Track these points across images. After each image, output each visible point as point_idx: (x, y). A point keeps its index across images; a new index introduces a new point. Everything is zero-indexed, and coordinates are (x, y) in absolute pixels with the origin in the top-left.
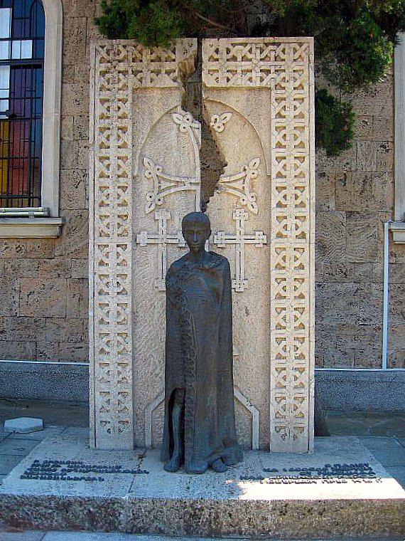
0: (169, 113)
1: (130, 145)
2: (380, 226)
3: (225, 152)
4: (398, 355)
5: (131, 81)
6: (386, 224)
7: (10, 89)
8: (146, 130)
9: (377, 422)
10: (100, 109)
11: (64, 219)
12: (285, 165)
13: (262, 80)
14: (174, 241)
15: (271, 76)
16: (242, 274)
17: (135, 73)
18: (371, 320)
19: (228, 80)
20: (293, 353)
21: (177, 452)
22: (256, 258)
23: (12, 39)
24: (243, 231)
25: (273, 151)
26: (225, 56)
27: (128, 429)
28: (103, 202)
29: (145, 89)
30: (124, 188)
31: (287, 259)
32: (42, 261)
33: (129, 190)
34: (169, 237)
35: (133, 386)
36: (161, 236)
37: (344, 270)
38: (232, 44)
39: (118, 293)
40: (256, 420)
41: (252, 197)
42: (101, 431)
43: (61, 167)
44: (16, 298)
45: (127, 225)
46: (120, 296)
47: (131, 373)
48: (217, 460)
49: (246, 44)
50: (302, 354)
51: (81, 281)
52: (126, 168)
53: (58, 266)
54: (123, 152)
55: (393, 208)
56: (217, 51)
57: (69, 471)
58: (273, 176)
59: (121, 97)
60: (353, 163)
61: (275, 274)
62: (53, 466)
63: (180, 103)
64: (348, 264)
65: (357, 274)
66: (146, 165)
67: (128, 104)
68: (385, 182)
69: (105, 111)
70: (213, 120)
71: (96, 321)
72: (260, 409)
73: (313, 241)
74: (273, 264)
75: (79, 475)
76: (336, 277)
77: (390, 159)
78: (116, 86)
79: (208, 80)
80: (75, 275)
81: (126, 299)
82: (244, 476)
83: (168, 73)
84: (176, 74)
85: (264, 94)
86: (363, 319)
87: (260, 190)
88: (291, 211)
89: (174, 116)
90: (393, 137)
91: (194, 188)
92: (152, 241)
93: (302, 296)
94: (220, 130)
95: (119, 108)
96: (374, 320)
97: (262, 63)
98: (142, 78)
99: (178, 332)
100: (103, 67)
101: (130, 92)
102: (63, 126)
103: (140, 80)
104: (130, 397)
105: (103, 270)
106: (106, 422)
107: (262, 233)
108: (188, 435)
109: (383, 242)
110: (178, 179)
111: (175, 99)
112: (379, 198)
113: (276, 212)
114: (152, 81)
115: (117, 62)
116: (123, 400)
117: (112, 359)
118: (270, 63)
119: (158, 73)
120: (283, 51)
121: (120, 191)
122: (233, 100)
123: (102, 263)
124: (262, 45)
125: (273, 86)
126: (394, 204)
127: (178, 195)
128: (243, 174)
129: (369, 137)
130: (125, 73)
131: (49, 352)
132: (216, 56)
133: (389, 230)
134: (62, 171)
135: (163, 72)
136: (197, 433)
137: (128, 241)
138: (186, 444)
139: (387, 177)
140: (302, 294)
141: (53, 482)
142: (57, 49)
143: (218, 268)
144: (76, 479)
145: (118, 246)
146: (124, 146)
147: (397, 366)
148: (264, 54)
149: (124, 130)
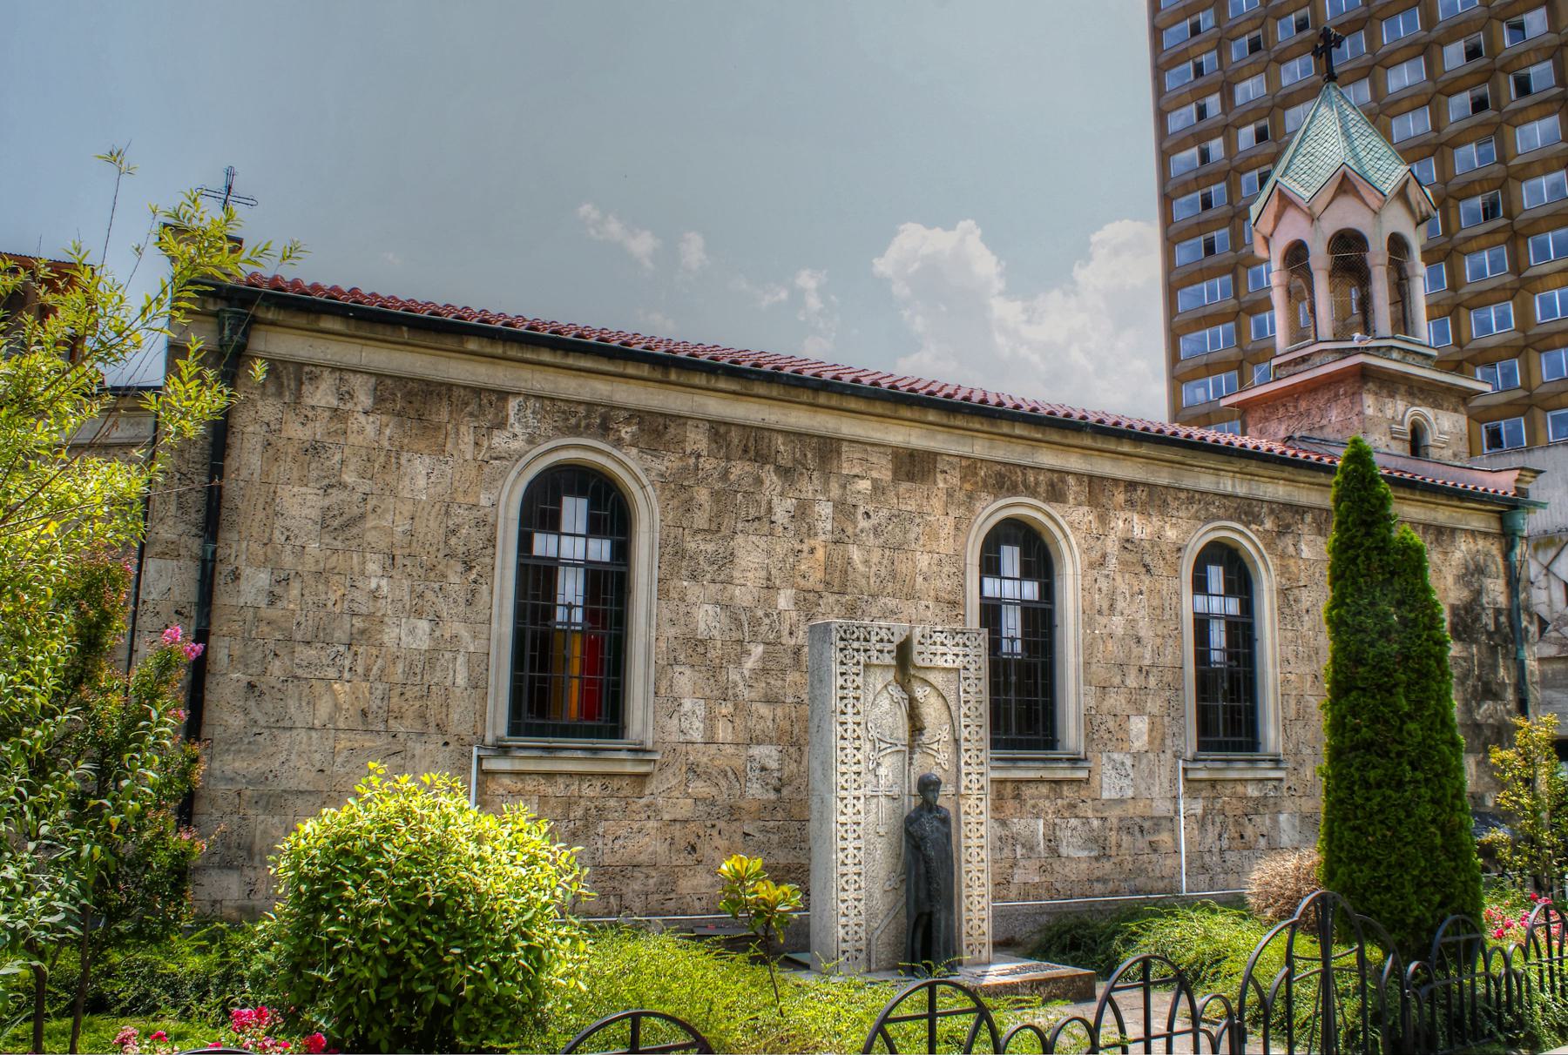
5: (862, 658)
10: (840, 681)
17: (866, 651)
27: (862, 956)
111: (890, 676)
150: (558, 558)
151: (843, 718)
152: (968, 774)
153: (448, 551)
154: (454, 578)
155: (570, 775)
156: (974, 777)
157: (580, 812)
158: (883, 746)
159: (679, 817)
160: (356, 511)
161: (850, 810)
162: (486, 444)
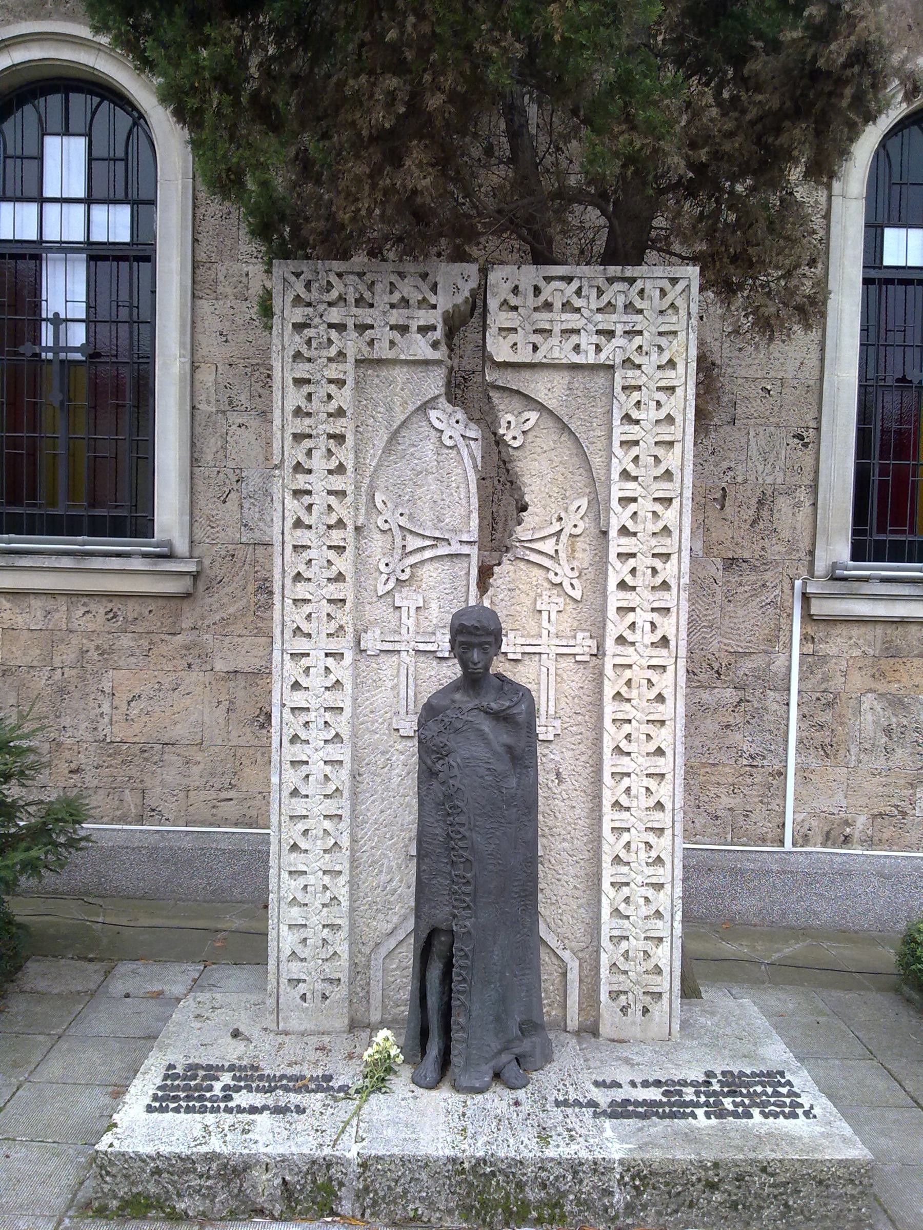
0: (424, 408)
2: (787, 587)
3: (525, 484)
4: (814, 823)
5: (353, 345)
6: (798, 583)
7: (88, 302)
8: (380, 440)
9: (779, 951)
10: (295, 398)
11: (200, 563)
13: (598, 349)
14: (429, 647)
16: (551, 712)
17: (362, 328)
18: (764, 758)
19: (535, 348)
20: (643, 855)
21: (434, 1050)
22: (575, 681)
23: (89, 201)
24: (553, 630)
25: (615, 488)
26: (531, 302)
27: (339, 993)
28: (299, 574)
29: (380, 362)
30: (340, 549)
32: (156, 638)
34: (419, 639)
35: (352, 910)
36: (406, 637)
37: (716, 666)
38: (545, 278)
39: (326, 741)
40: (573, 976)
41: (573, 569)
42: (290, 996)
43: (194, 461)
44: (106, 708)
46: (330, 747)
47: (347, 888)
48: (509, 1062)
50: (659, 857)
51: (232, 676)
52: (342, 510)
53: (187, 648)
54: (337, 483)
55: (812, 553)
56: (515, 290)
57: (238, 1089)
58: (613, 533)
59: (334, 375)
60: (740, 469)
61: (610, 709)
62: (205, 1078)
63: (443, 390)
64: (723, 654)
65: (740, 673)
66: (380, 505)
68: (798, 505)
69: (303, 403)
70: (504, 424)
71: (286, 793)
73: (683, 652)
75: (258, 1100)
76: (702, 677)
77: (809, 461)
78: (324, 353)
80: (220, 666)
81: (341, 752)
82: (561, 1098)
83: (424, 330)
84: (438, 334)
85: (600, 379)
86: (751, 756)
88: (643, 598)
89: (433, 414)
90: (818, 420)
91: (466, 550)
92: (389, 646)
93: (660, 752)
94: (516, 444)
96: (770, 756)
97: (599, 317)
98: (373, 340)
99: (441, 824)
100: (298, 314)
101: (349, 366)
102: (197, 383)
103: (371, 343)
105: (299, 698)
106: (299, 981)
108: (458, 1019)
109: (790, 616)
110: (437, 534)
111: (434, 383)
112: (786, 534)
113: (615, 599)
114: (392, 343)
115: (325, 306)
116: (330, 939)
117: (314, 861)
118: (614, 317)
119: (404, 329)
120: (641, 292)
121: (332, 555)
122: (548, 389)
123: (296, 686)
124: (601, 282)
126: (814, 545)
128: (557, 527)
129: (771, 420)
130: (340, 327)
131: (169, 808)
132: (513, 301)
133: (804, 594)
134: (197, 470)
136: (474, 1014)
137: (344, 644)
138: (455, 1035)
139: (802, 495)
140: (659, 748)
141: (210, 1118)
142: (183, 228)
143: (514, 715)
144: (253, 1110)
145: (327, 655)
146: (341, 469)
147: (812, 841)
148: (605, 299)
149: (340, 438)
150: (41, 241)
151: (301, 481)
152: (623, 610)
155: (52, 595)
157: (70, 656)
158: (413, 543)
159: (242, 665)
161: (315, 681)
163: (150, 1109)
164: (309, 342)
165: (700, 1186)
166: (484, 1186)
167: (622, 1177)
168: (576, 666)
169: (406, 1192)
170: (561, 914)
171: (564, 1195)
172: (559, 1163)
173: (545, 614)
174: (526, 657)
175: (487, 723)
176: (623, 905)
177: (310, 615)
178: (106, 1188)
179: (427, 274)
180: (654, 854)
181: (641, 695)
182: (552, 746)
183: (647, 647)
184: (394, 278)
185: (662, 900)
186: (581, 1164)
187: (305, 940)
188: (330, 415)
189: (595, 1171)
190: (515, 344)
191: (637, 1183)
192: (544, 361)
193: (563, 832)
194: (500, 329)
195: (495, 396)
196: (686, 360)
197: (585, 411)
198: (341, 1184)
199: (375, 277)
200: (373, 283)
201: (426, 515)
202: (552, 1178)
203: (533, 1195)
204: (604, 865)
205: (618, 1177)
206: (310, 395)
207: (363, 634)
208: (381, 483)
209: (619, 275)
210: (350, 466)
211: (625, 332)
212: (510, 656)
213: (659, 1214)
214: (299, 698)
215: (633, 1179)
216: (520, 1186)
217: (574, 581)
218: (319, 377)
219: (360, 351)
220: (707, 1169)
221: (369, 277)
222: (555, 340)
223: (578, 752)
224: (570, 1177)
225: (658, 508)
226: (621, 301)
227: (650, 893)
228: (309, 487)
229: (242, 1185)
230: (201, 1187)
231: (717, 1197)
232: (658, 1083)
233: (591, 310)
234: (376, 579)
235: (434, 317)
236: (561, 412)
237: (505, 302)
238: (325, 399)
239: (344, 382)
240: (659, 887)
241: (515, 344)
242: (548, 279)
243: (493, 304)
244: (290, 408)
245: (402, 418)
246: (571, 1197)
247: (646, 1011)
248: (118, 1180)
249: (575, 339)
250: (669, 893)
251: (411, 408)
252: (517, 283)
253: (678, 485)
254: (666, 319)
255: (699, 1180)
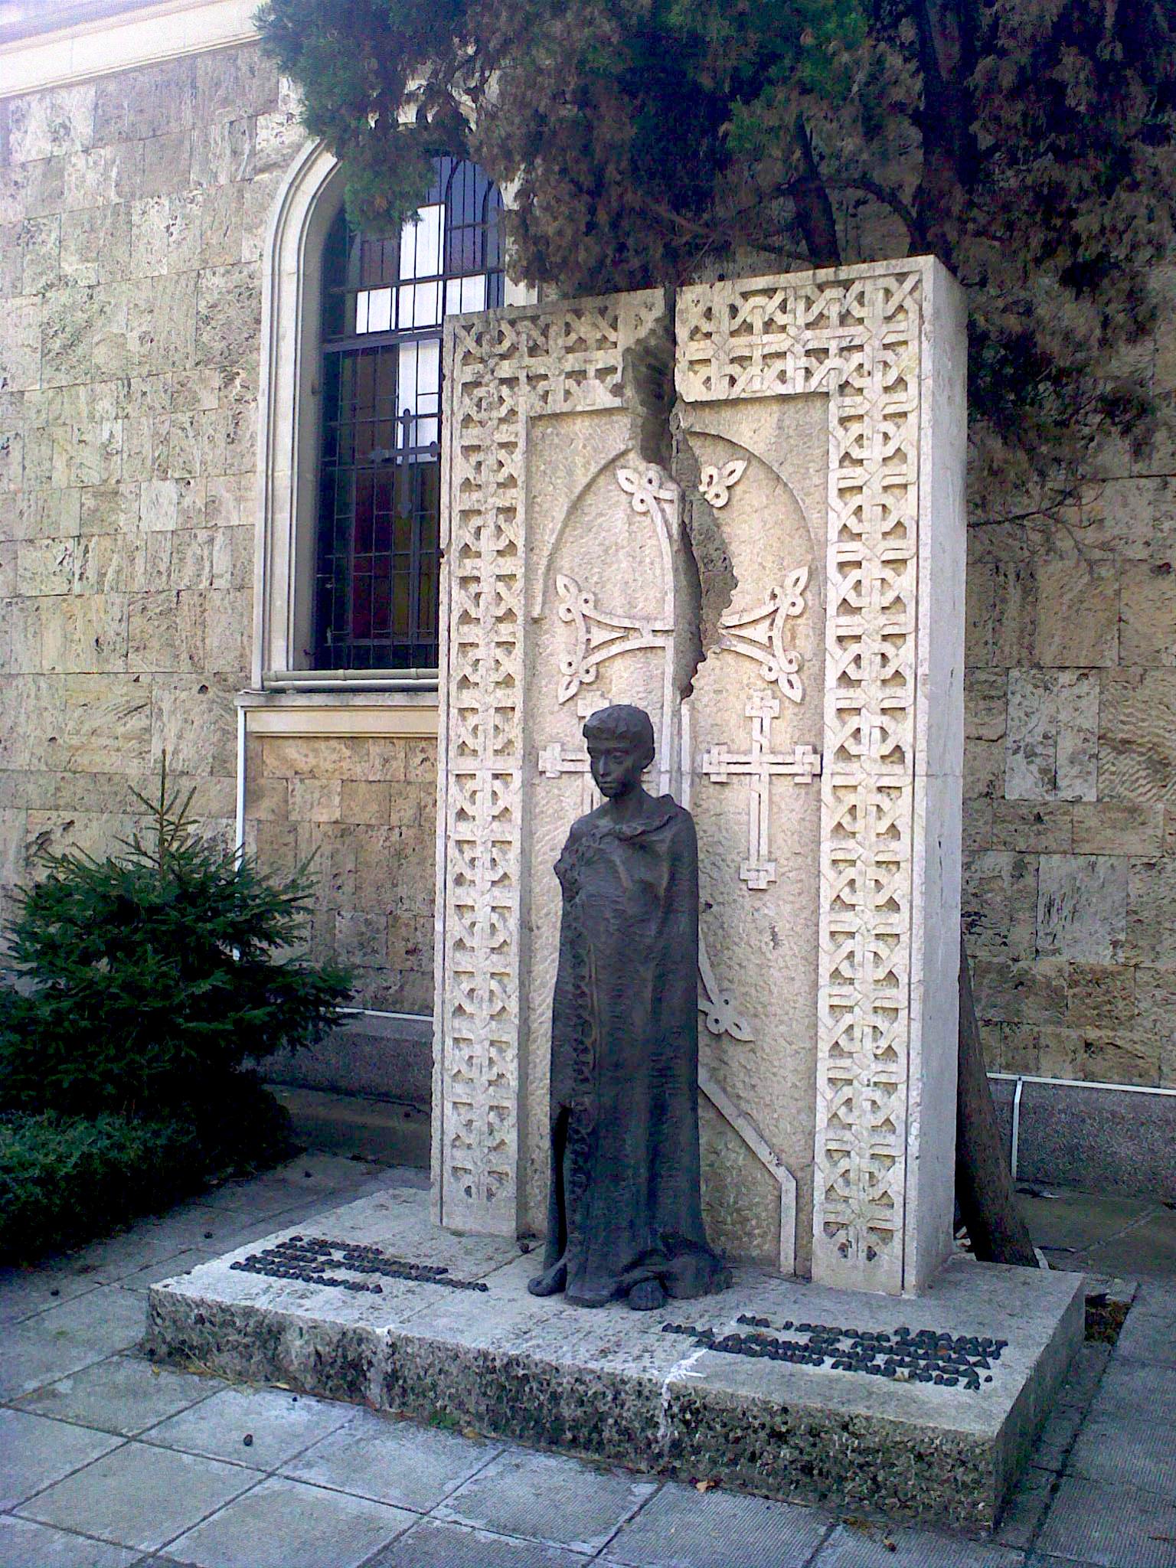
1: (521, 548)
5: (524, 400)
12: (859, 582)
15: (829, 363)
16: (764, 851)
19: (733, 381)
20: (869, 1044)
26: (726, 324)
29: (556, 416)
31: (859, 813)
33: (519, 650)
39: (494, 883)
40: (789, 1200)
42: (453, 1189)
45: (514, 731)
46: (496, 891)
49: (775, 290)
52: (513, 600)
54: (508, 565)
56: (708, 314)
59: (504, 438)
66: (561, 590)
67: (518, 455)
70: (705, 479)
71: (449, 944)
72: (799, 1175)
74: (827, 824)
78: (495, 414)
79: (689, 386)
83: (603, 373)
87: (805, 645)
88: (871, 695)
89: (622, 474)
91: (659, 641)
94: (720, 503)
95: (501, 464)
97: (809, 334)
98: (547, 392)
100: (467, 374)
101: (520, 427)
104: (512, 1119)
105: (464, 831)
107: (810, 748)
110: (627, 623)
111: (620, 435)
113: (834, 697)
115: (497, 359)
118: (827, 333)
121: (499, 654)
122: (753, 430)
123: (461, 814)
124: (809, 291)
125: (833, 387)
127: (628, 660)
130: (511, 382)
132: (706, 327)
135: (591, 373)
148: (816, 310)
153: (200, 357)
154: (209, 400)
156: (868, 722)
160: (80, 317)
162: (247, 147)
163: (232, 1268)
164: (479, 405)
165: (763, 1435)
166: (518, 1392)
167: (670, 1406)
168: (797, 790)
169: (434, 1386)
170: (777, 1120)
171: (602, 1418)
172: (599, 1377)
173: (757, 723)
174: (735, 779)
175: (620, 851)
176: (843, 1109)
177: (476, 728)
178: (157, 1330)
179: (606, 308)
180: (883, 1044)
181: (868, 827)
182: (766, 897)
183: (875, 761)
184: (569, 318)
185: (895, 1106)
186: (623, 1382)
187: (470, 1122)
188: (499, 485)
189: (640, 1393)
190: (709, 379)
191: (688, 1416)
192: (743, 395)
193: (779, 1012)
194: (691, 362)
195: (693, 442)
196: (919, 377)
197: (798, 454)
198: (370, 1363)
199: (549, 319)
200: (547, 326)
201: (616, 600)
202: (590, 1393)
203: (568, 1411)
204: (820, 1055)
205: (666, 1405)
206: (479, 464)
207: (541, 753)
208: (564, 562)
209: (832, 278)
210: (520, 543)
211: (842, 349)
212: (714, 778)
213: (714, 1462)
214: (464, 831)
215: (683, 1410)
216: (555, 1397)
217: (791, 677)
218: (489, 443)
219: (532, 407)
220: (772, 1414)
221: (542, 322)
222: (755, 369)
223: (797, 906)
224: (610, 1398)
225: (888, 573)
226: (834, 312)
227: (878, 1095)
228: (476, 573)
229: (276, 1348)
230: (239, 1344)
231: (785, 1452)
232: (804, 1328)
233: (799, 328)
234: (557, 683)
235: (612, 357)
236: (770, 458)
237: (697, 329)
238: (495, 467)
239: (515, 444)
240: (890, 1088)
241: (709, 379)
242: (745, 296)
243: (682, 332)
244: (457, 481)
245: (585, 481)
246: (611, 1421)
247: (871, 1255)
248: (167, 1323)
249: (778, 365)
250: (904, 1097)
251: (594, 469)
252: (709, 304)
253: (913, 541)
254: (892, 326)
255: (763, 1426)
